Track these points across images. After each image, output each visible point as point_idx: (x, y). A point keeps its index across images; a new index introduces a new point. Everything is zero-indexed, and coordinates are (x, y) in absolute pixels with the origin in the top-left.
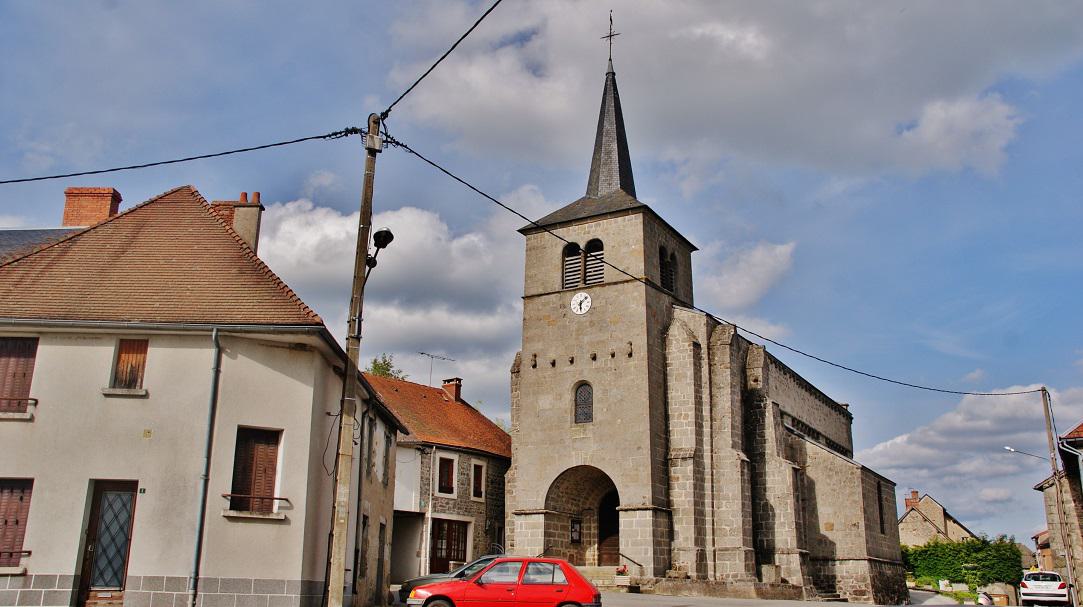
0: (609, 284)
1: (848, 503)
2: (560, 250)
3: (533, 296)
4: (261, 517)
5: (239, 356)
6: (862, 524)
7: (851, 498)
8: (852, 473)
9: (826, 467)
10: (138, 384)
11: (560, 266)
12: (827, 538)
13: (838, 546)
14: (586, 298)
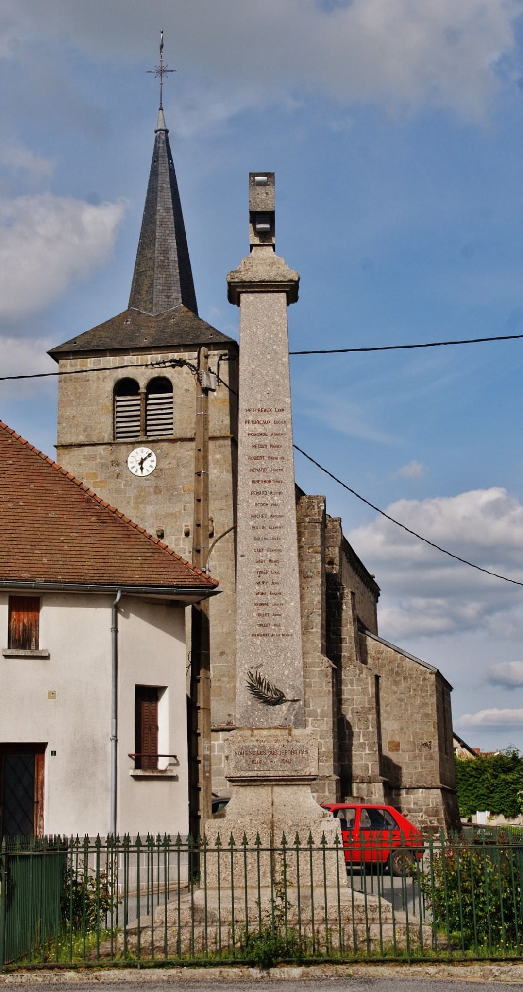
0: (182, 440)
1: (418, 717)
2: (110, 386)
3: (71, 446)
4: (147, 774)
5: (131, 615)
6: (435, 743)
7: (422, 711)
8: (425, 679)
9: (392, 670)
10: (33, 643)
11: (111, 408)
12: (391, 761)
13: (404, 771)
14: (149, 455)
